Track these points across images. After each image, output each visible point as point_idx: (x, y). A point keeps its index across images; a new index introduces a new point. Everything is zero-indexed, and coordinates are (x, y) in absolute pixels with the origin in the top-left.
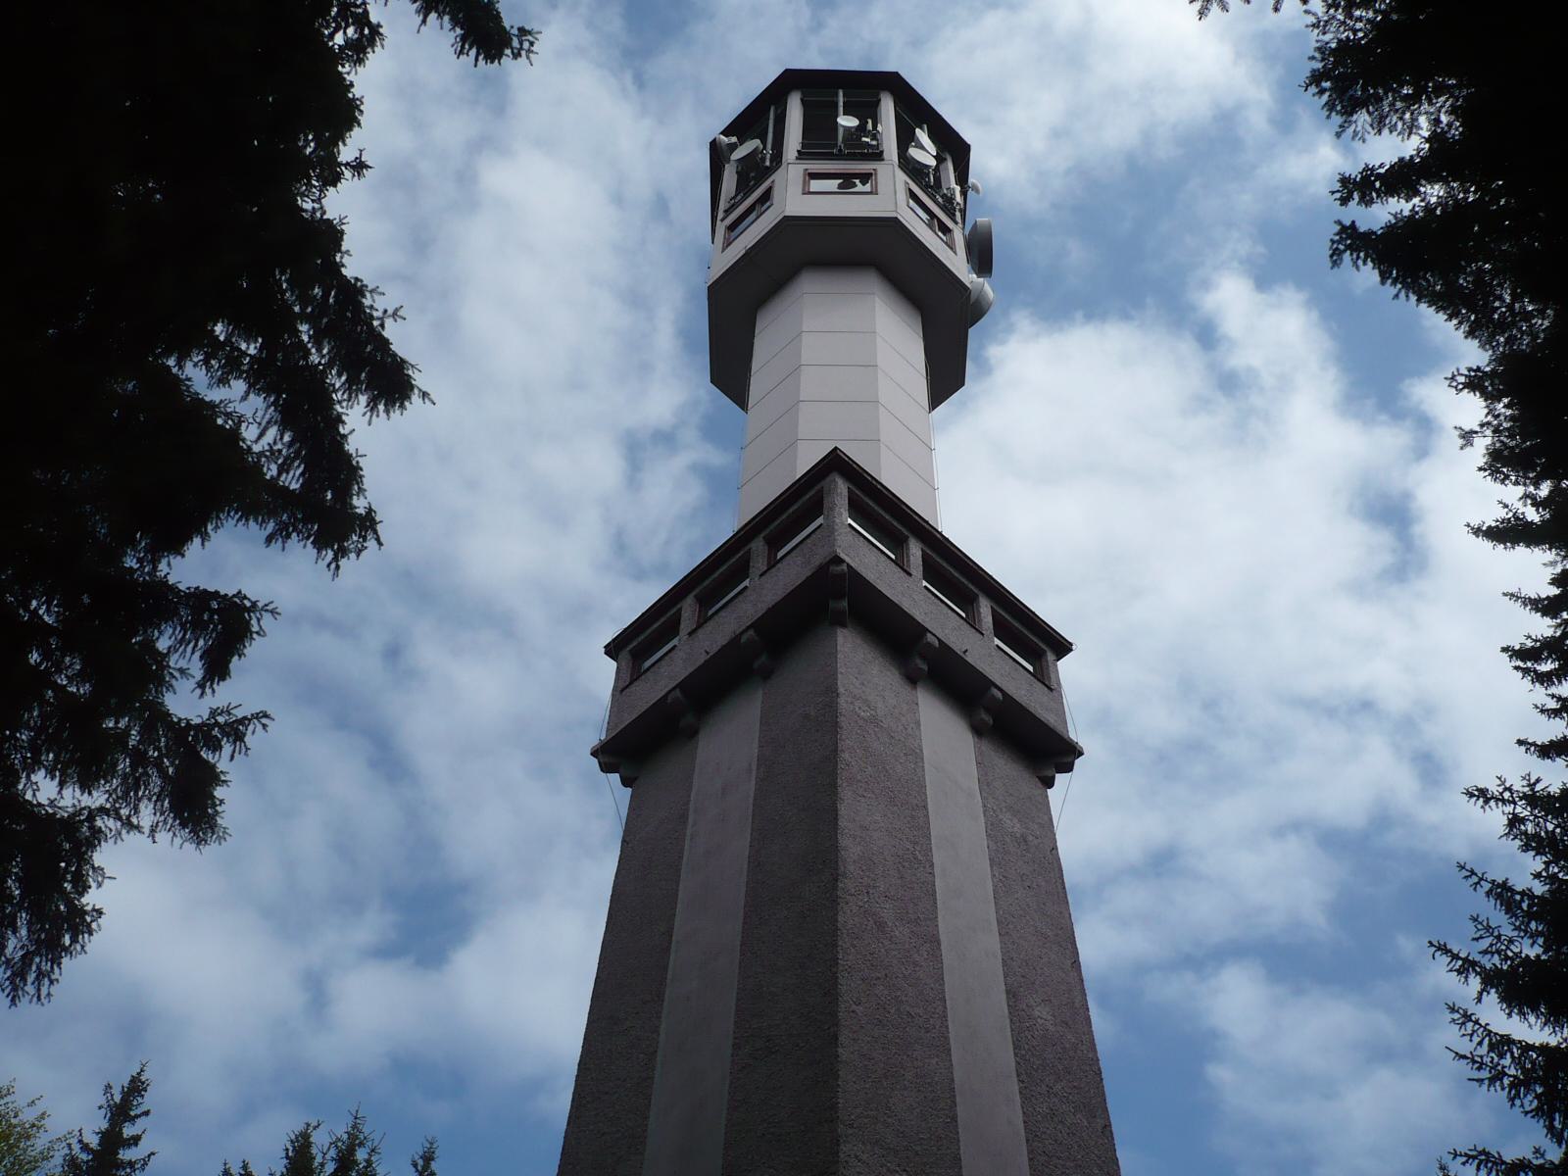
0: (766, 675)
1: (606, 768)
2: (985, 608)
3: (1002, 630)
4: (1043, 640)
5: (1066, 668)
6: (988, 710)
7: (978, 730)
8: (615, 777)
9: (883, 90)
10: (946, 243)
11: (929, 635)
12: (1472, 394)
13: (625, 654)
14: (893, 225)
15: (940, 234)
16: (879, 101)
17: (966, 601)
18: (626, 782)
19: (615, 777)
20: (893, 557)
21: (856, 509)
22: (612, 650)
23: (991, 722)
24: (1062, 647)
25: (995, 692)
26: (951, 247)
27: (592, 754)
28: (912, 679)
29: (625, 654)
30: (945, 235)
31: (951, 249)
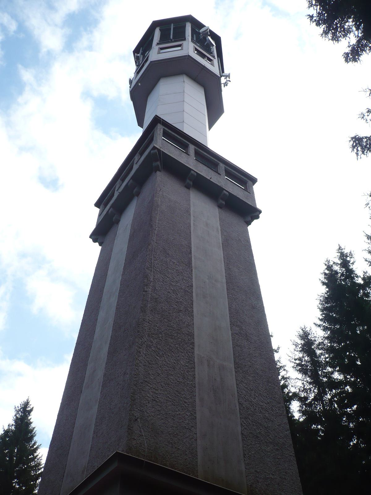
0: (138, 194)
1: (95, 241)
2: (192, 148)
3: (228, 174)
4: (219, 161)
5: (256, 188)
6: (222, 199)
7: (220, 207)
8: (97, 244)
9: (190, 22)
10: (211, 64)
11: (224, 191)
12: (345, 62)
13: (102, 206)
14: (189, 57)
15: (207, 61)
16: (185, 25)
17: (185, 147)
18: (100, 245)
19: (97, 244)
20: (244, 188)
21: (165, 134)
22: (97, 205)
23: (224, 203)
24: (254, 180)
25: (192, 172)
26: (212, 64)
27: (90, 237)
28: (188, 187)
29: (102, 206)
30: (210, 62)
31: (213, 65)
